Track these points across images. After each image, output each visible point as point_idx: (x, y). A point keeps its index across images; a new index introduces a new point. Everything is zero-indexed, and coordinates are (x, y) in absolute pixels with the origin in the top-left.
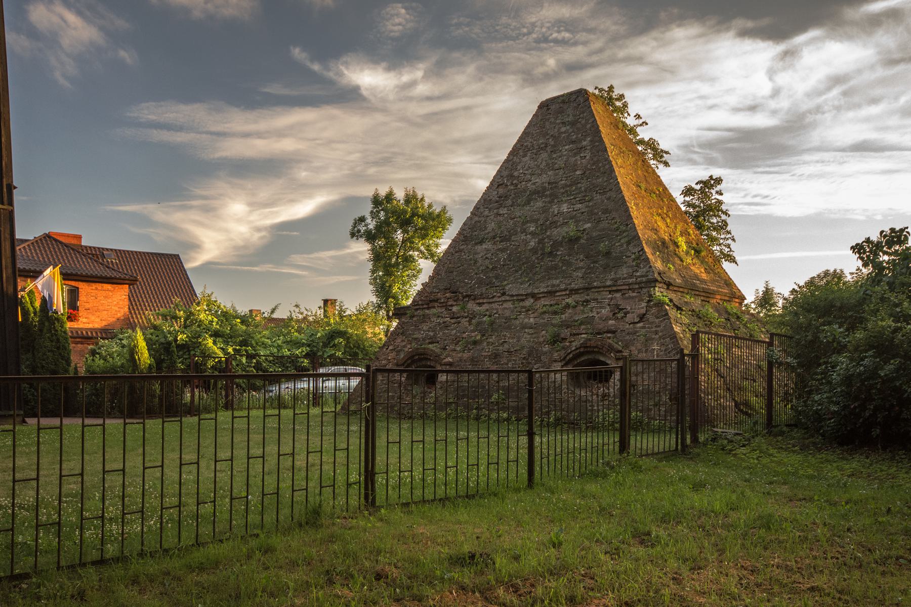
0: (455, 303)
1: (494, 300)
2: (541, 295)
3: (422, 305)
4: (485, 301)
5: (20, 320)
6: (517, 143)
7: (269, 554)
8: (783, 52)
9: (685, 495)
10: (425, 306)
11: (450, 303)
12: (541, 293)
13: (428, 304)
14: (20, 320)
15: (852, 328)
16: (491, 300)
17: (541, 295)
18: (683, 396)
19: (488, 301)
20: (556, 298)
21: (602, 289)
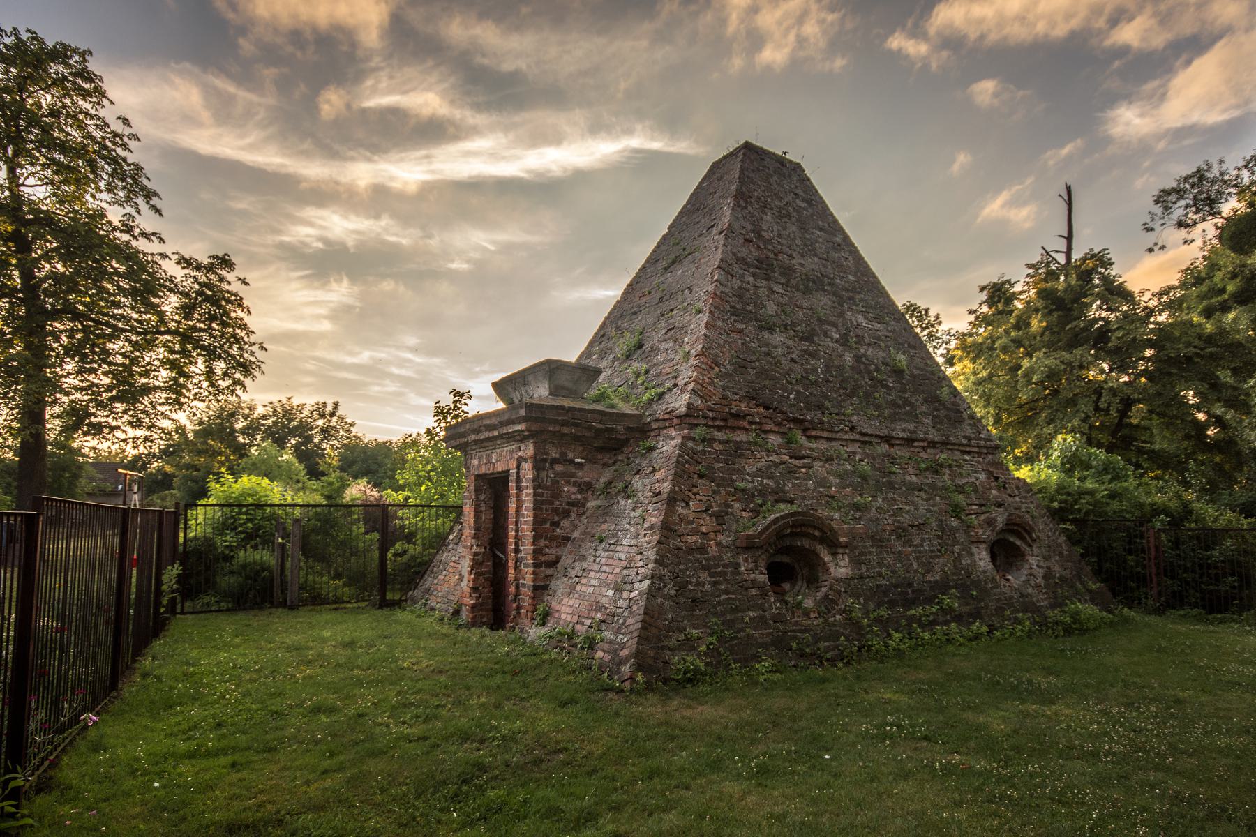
0: (776, 429)
1: (838, 436)
2: (898, 442)
3: (714, 419)
4: (825, 434)
5: (135, 571)
6: (834, 217)
7: (347, 639)
8: (1130, 103)
9: (461, 523)
10: (718, 423)
11: (768, 427)
12: (898, 438)
13: (725, 420)
14: (135, 571)
15: (1053, 606)
16: (834, 436)
17: (898, 442)
18: (460, 445)
19: (830, 435)
20: (912, 449)
21: (956, 447)
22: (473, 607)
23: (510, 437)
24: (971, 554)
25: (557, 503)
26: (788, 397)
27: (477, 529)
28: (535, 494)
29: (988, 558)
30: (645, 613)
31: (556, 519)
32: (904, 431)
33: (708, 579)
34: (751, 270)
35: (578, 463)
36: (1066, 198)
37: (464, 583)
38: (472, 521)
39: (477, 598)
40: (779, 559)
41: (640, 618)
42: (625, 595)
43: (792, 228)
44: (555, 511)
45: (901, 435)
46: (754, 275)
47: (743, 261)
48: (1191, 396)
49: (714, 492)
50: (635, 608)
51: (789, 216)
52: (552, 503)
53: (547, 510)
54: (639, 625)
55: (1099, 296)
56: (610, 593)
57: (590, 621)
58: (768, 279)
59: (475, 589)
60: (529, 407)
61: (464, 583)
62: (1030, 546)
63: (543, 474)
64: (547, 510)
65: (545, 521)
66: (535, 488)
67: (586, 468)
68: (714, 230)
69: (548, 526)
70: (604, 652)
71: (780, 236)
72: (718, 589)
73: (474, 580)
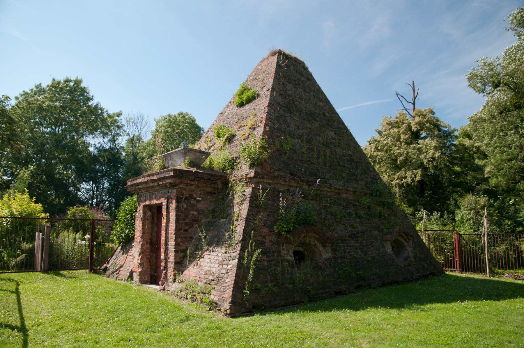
22: (140, 272)
23: (165, 186)
24: (384, 247)
25: (187, 220)
26: (301, 170)
27: (143, 233)
28: (176, 215)
29: (391, 249)
30: (236, 276)
31: (186, 228)
32: (353, 188)
33: (266, 259)
34: (283, 108)
35: (198, 200)
36: (412, 86)
37: (136, 260)
38: (140, 229)
39: (142, 268)
40: (298, 249)
41: (234, 278)
42: (225, 267)
43: (300, 90)
44: (186, 224)
45: (352, 189)
46: (284, 111)
47: (279, 104)
48: (49, 193)
49: (268, 215)
50: (230, 273)
51: (299, 84)
52: (185, 220)
53: (182, 223)
54: (233, 282)
55: (121, 162)
56: (217, 265)
57: (206, 280)
58: (291, 113)
59: (141, 264)
60: (175, 171)
61: (136, 260)
62: (408, 242)
63: (181, 205)
64: (182, 223)
65: (181, 229)
66: (176, 212)
67: (202, 202)
68: (265, 89)
69: (182, 231)
70: (215, 295)
71: (295, 93)
72: (271, 264)
73: (141, 259)
